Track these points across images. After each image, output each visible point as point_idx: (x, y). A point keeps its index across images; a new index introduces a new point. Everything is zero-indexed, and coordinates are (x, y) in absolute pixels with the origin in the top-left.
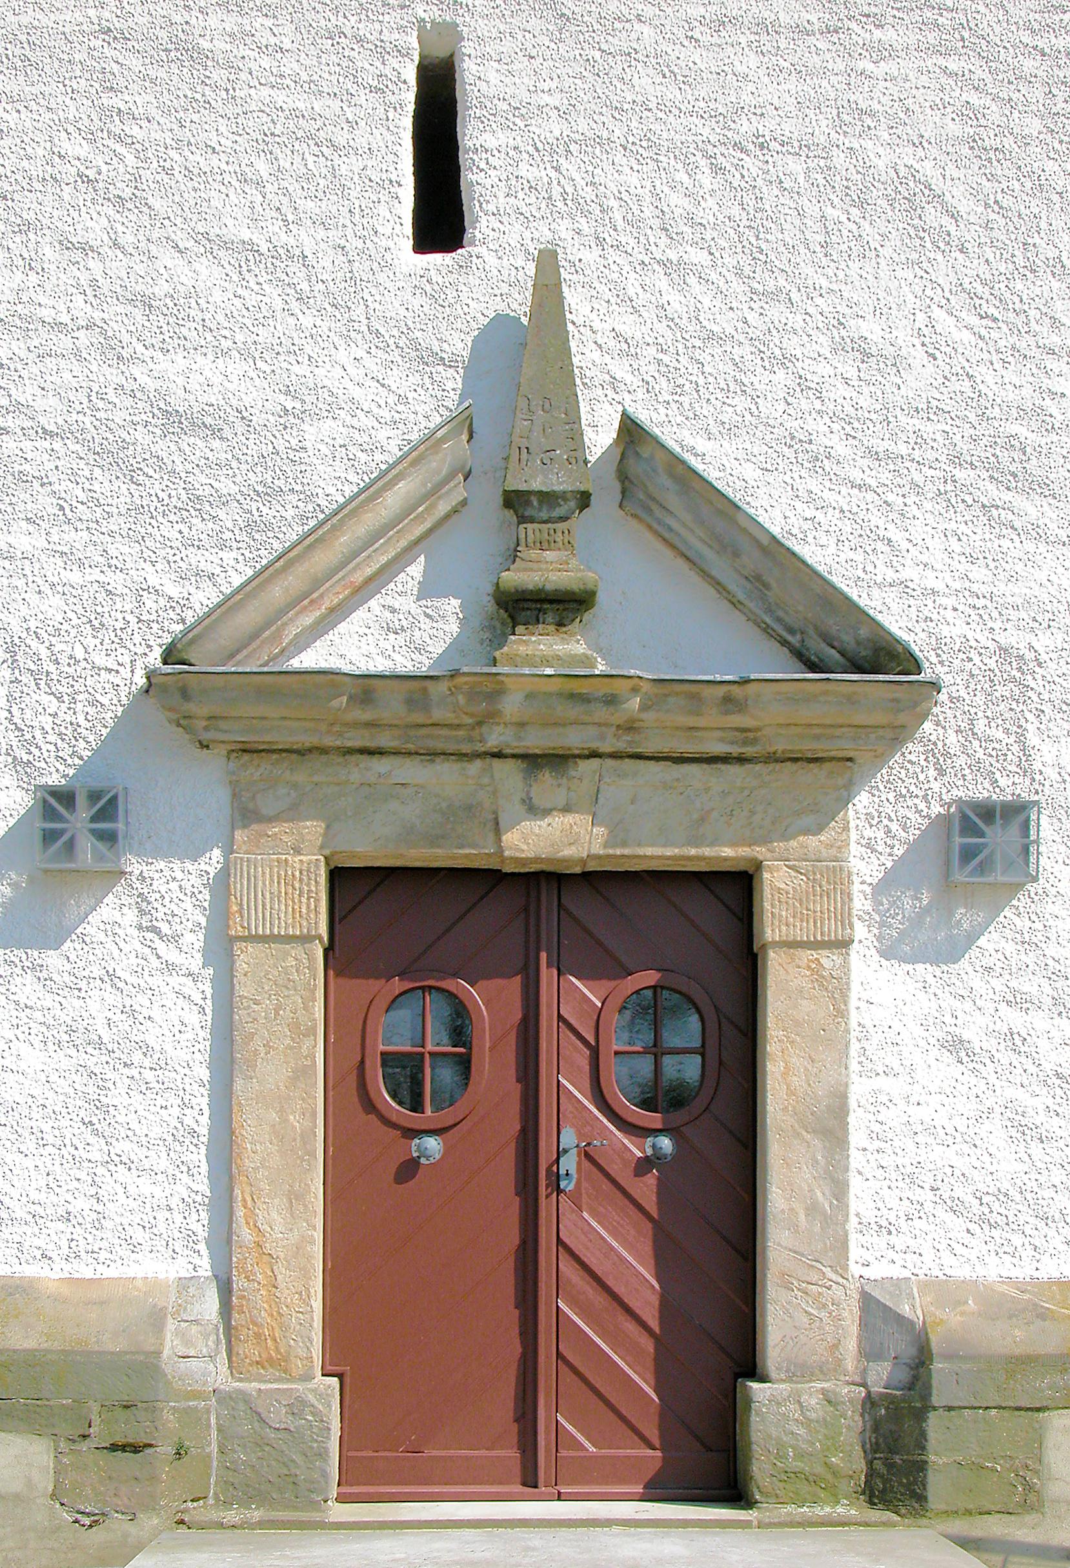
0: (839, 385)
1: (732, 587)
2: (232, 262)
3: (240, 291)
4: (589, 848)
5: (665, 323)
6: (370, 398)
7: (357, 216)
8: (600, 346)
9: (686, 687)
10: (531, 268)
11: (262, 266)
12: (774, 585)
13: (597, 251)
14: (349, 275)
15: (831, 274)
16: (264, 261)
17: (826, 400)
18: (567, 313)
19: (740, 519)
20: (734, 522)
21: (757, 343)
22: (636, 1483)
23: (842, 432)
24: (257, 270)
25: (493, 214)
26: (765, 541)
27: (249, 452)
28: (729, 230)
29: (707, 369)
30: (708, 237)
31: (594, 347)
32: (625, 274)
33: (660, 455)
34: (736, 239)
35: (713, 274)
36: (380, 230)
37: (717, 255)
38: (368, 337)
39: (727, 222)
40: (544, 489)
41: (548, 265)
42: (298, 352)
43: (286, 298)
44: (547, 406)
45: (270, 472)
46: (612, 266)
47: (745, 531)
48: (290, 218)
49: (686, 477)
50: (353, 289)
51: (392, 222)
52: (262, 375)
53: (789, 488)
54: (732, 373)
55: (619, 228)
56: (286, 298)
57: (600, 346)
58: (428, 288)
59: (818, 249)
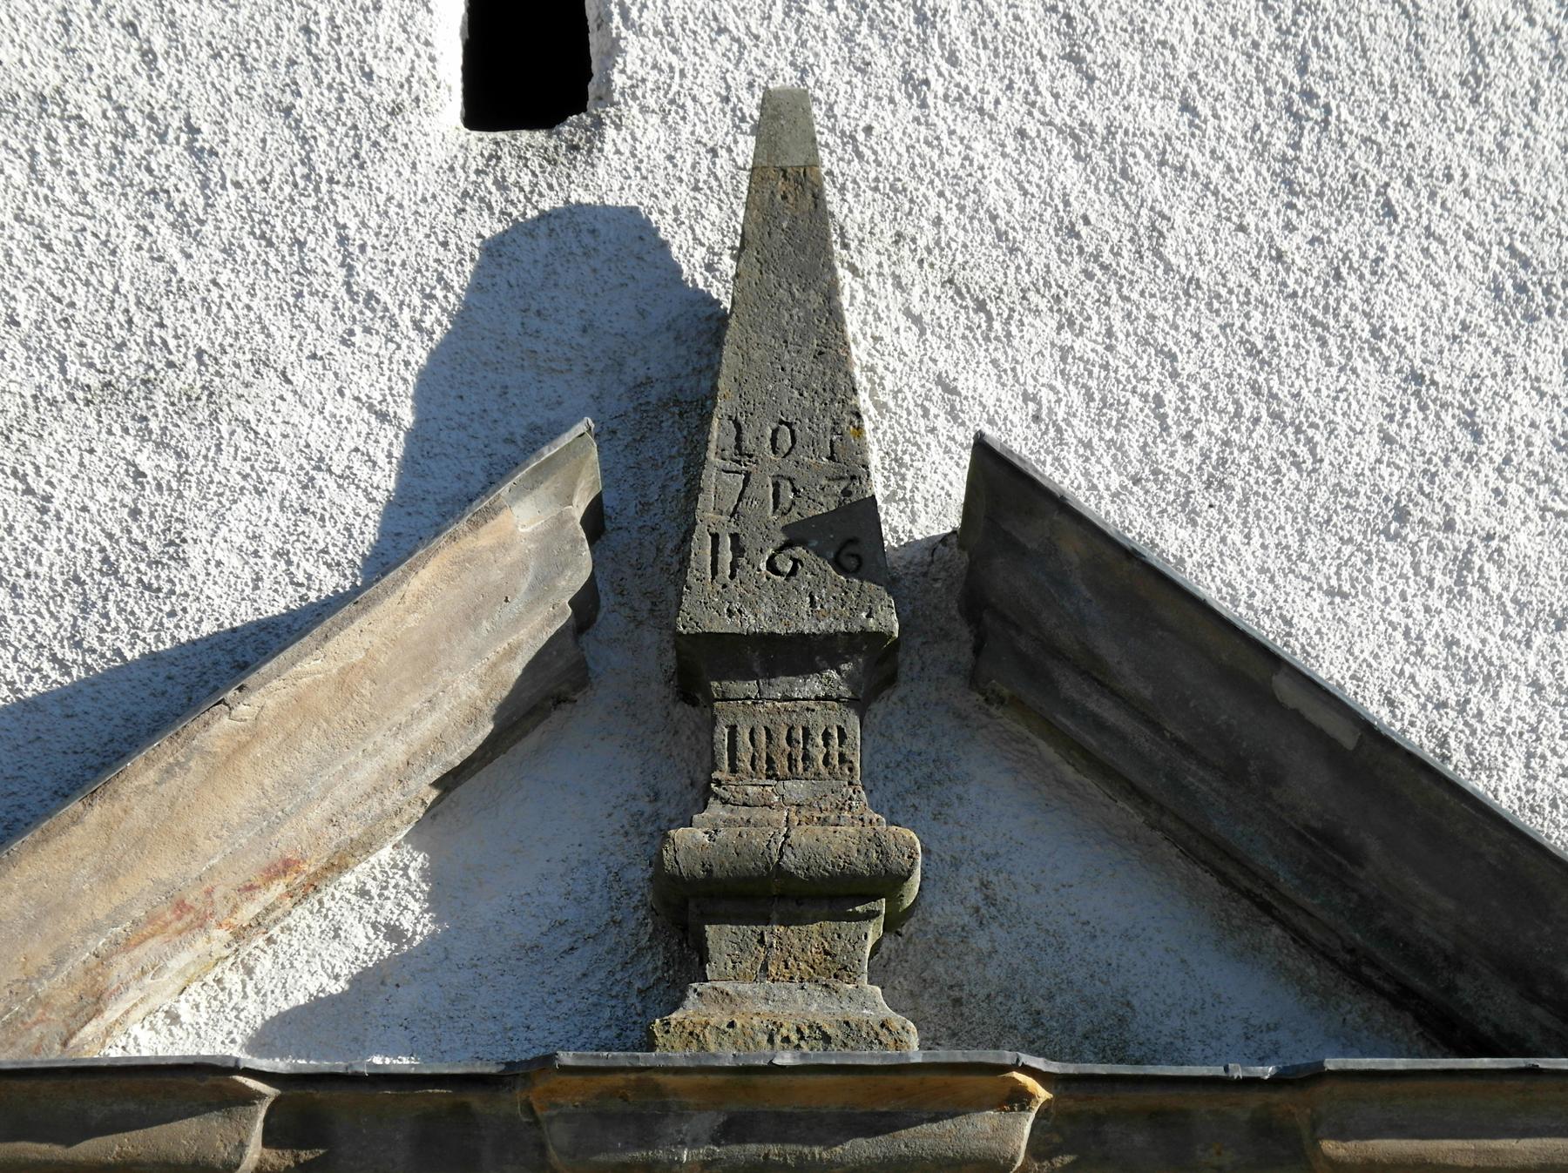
0: (1519, 395)
1: (1264, 860)
2: (13, 143)
3: (31, 209)
4: (716, 796)
5: (1077, 264)
6: (349, 444)
7: (324, 38)
8: (917, 320)
9: (1153, 1097)
10: (746, 147)
11: (88, 152)
12: (1374, 847)
13: (907, 110)
14: (300, 170)
15: (1489, 144)
16: (92, 140)
17: (1487, 429)
18: (837, 248)
19: (1283, 686)
20: (1266, 700)
21: (1307, 305)
22: (1332, 1163)
23: (1530, 501)
24: (76, 163)
25: (657, 33)
26: (1349, 740)
27: (43, 571)
28: (1232, 56)
29: (1187, 366)
30: (1181, 72)
31: (903, 322)
32: (979, 159)
33: (1072, 548)
34: (1251, 73)
35: (1194, 154)
36: (380, 70)
37: (1204, 110)
38: (346, 306)
39: (1229, 39)
40: (780, 629)
41: (783, 121)
42: (172, 343)
43: (144, 222)
44: (785, 440)
45: (94, 616)
46: (945, 142)
47: (1296, 718)
48: (159, 44)
49: (1141, 588)
50: (312, 201)
51: (410, 54)
52: (79, 394)
53: (1398, 636)
54: (1246, 374)
55: (961, 56)
56: (144, 222)
57: (917, 320)
58: (496, 198)
59: (1456, 90)
